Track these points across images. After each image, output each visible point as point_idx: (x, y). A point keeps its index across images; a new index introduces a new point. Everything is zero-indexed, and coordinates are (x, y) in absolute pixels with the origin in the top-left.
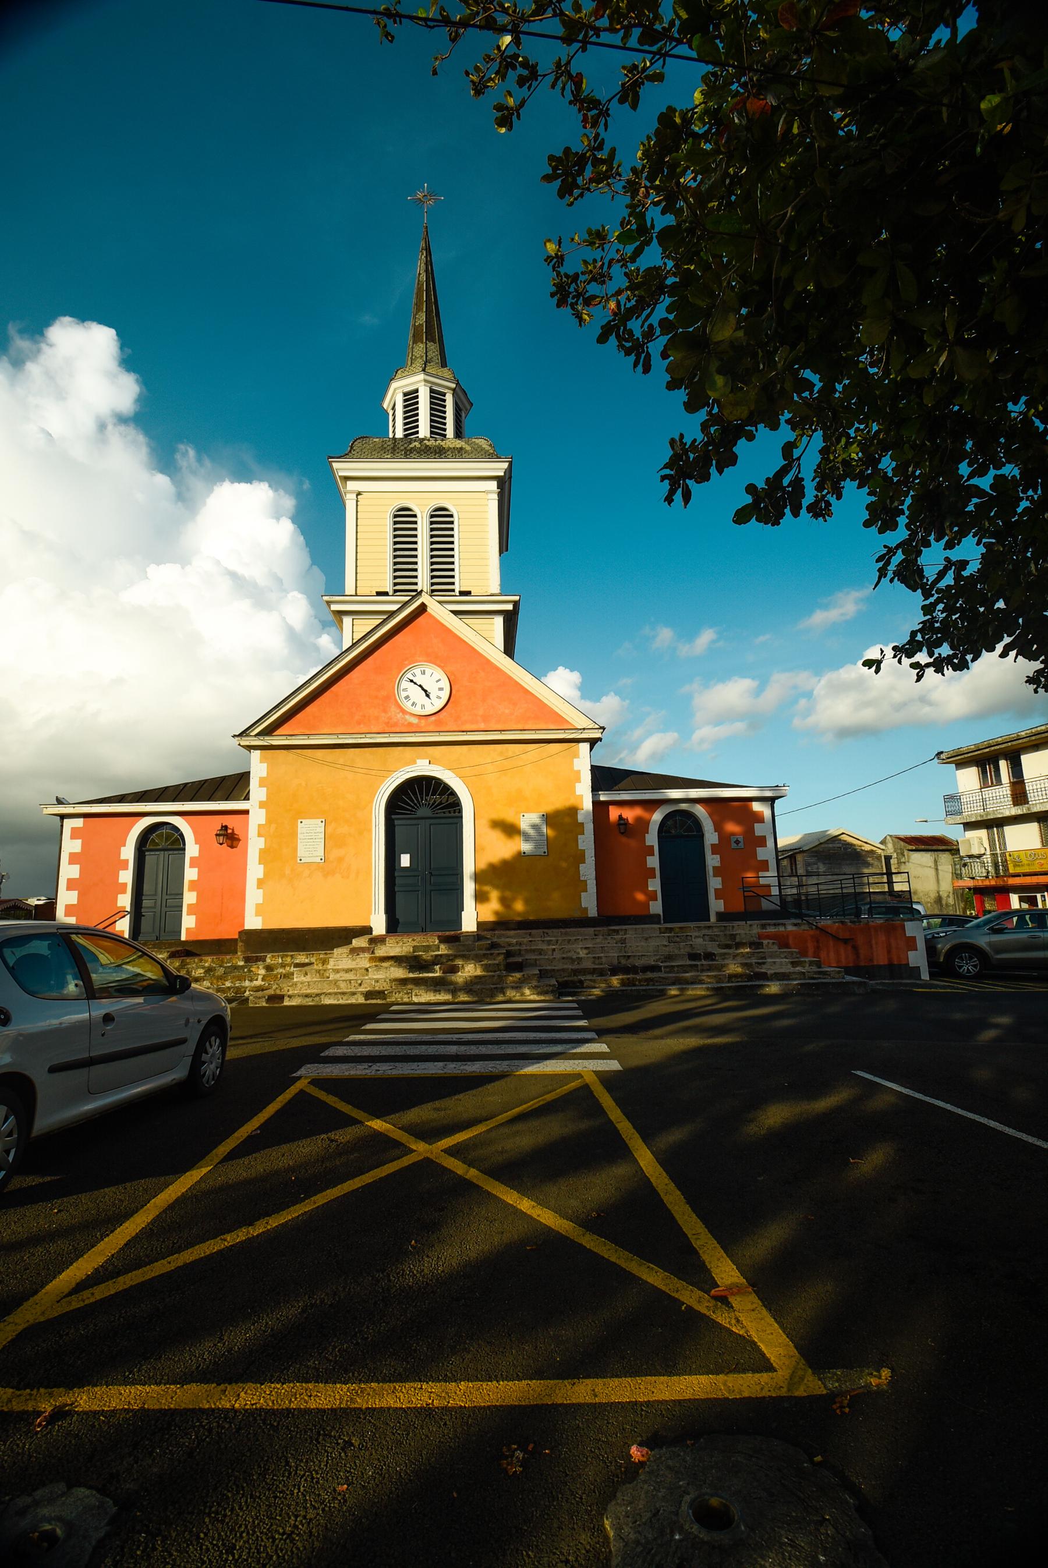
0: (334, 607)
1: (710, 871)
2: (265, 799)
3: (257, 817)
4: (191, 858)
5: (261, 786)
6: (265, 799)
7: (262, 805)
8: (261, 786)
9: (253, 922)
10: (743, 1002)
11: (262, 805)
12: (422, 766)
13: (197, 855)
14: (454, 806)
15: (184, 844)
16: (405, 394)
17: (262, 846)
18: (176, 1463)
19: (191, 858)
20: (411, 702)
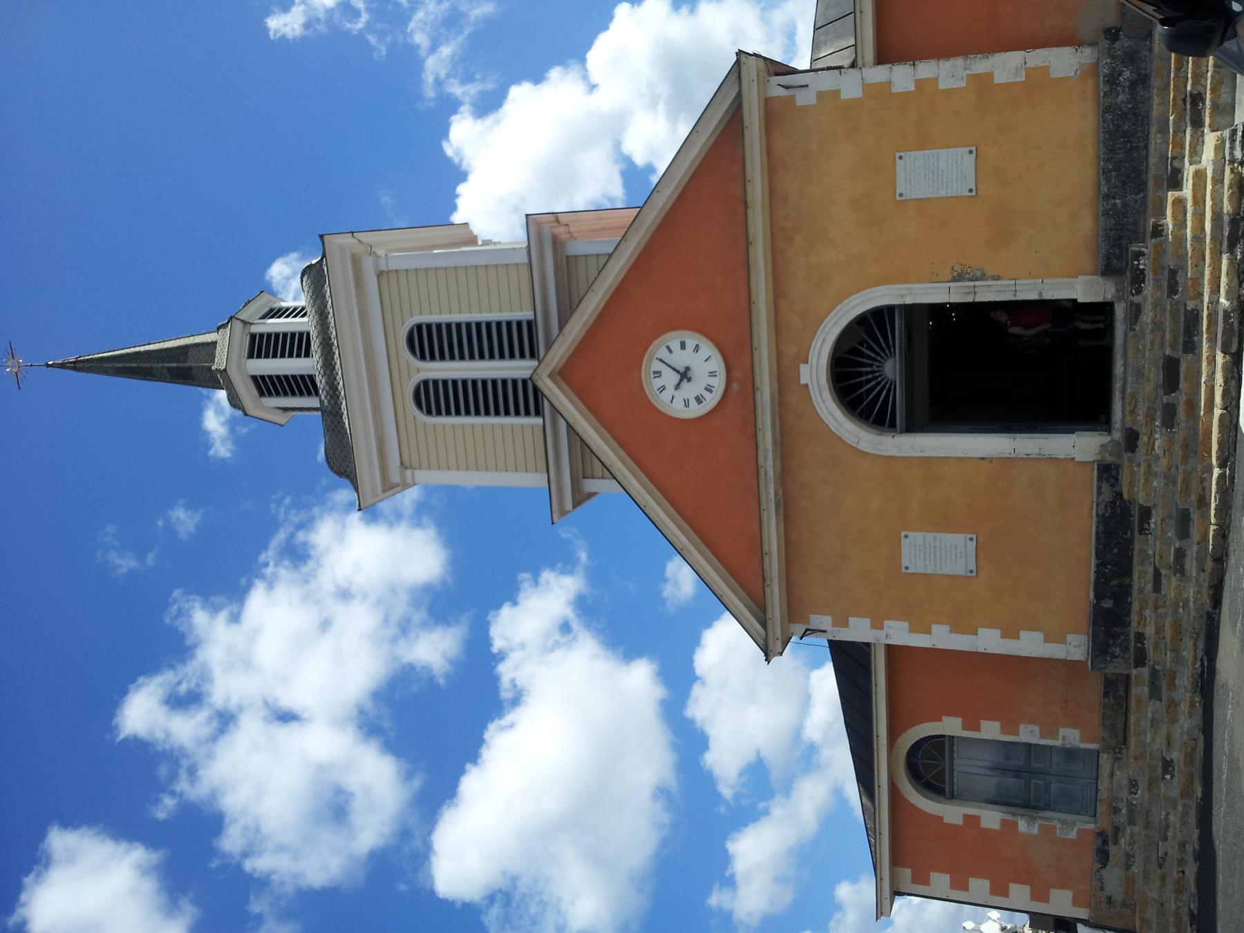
0: (569, 504)
1: (981, 65)
2: (868, 621)
3: (899, 633)
4: (964, 729)
5: (846, 625)
6: (868, 621)
7: (877, 625)
8: (846, 625)
9: (1075, 647)
10: (1178, 14)
11: (877, 625)
12: (815, 372)
13: (959, 720)
14: (874, 323)
15: (943, 736)
16: (262, 394)
17: (946, 628)
18: (1122, 819)
19: (964, 729)
20: (706, 394)
